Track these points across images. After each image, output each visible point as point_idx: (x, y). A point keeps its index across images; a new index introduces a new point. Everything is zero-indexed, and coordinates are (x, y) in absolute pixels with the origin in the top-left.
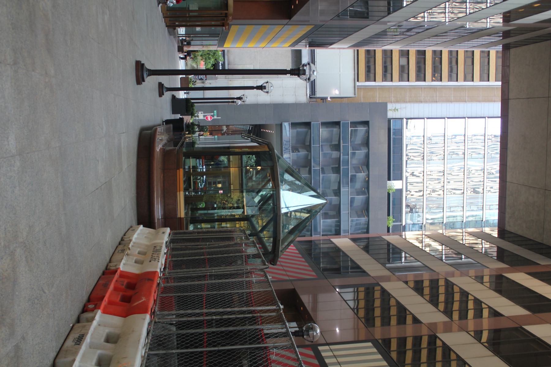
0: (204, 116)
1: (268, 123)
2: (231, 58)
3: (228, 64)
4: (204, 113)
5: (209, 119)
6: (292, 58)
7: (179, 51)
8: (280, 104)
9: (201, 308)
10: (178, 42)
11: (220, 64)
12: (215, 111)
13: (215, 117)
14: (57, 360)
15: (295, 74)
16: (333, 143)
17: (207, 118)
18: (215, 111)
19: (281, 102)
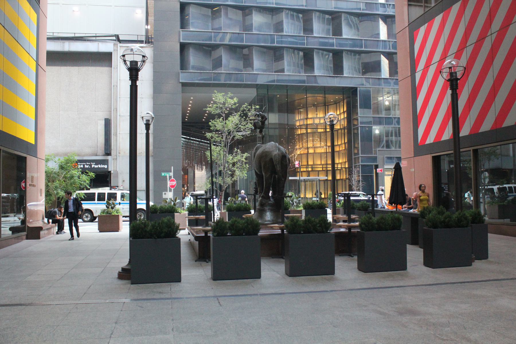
0: (170, 191)
1: (180, 102)
2: (88, 150)
3: (97, 155)
4: (167, 191)
5: (174, 183)
6: (83, 66)
7: (38, 237)
8: (154, 83)
9: (372, 176)
10: (17, 238)
11: (96, 166)
12: (163, 174)
13: (172, 174)
14: (192, 5)
15: (137, 75)
16: (210, 14)
17: (172, 186)
18: (163, 174)
19: (152, 82)
